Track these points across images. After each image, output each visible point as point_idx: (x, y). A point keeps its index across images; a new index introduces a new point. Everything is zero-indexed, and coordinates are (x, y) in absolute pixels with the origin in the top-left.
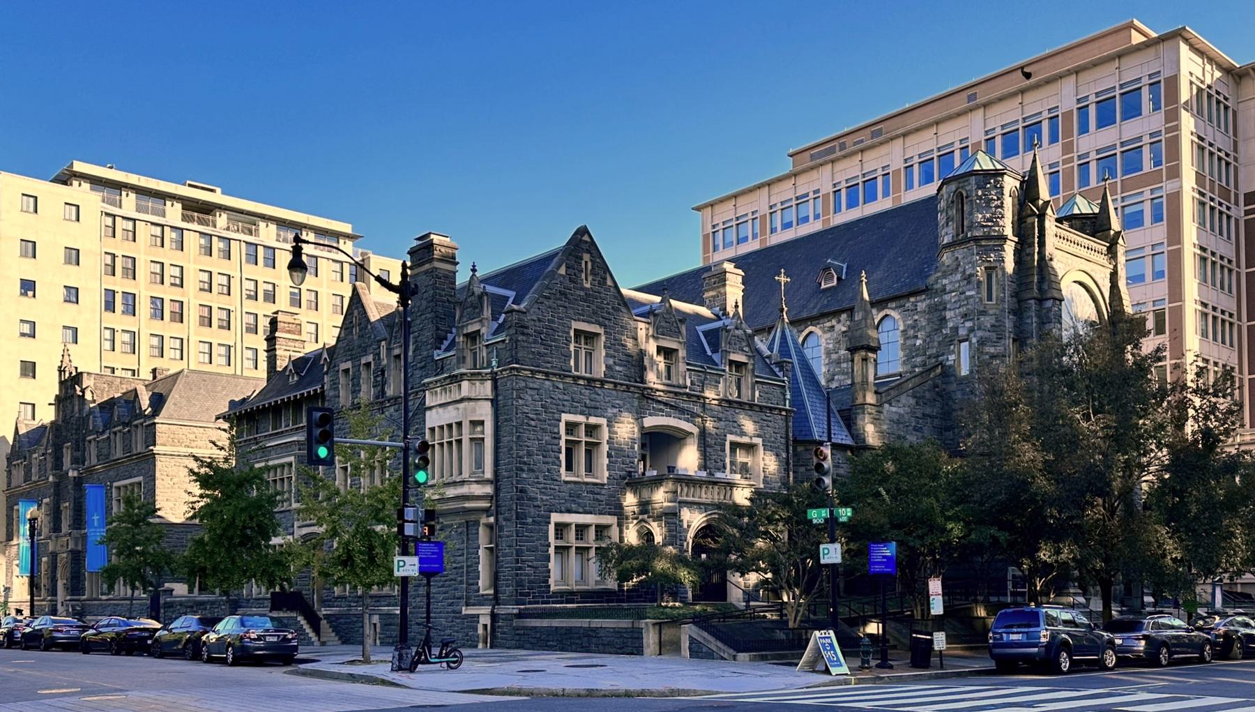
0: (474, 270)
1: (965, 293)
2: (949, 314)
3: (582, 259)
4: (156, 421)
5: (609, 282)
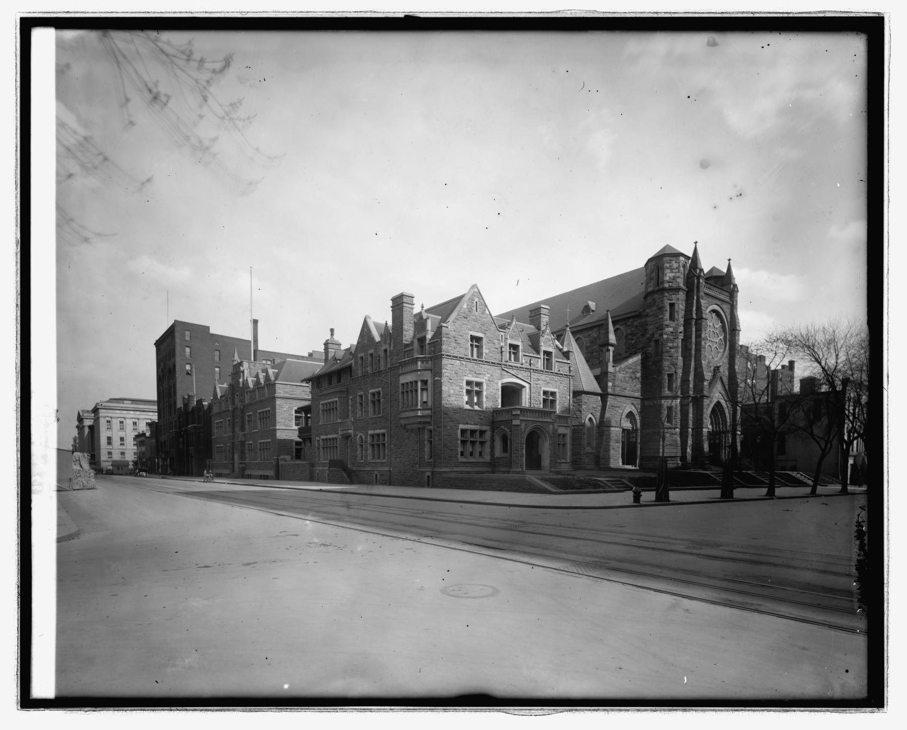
0: (422, 307)
1: (658, 316)
2: (649, 327)
3: (474, 300)
4: (276, 382)
5: (487, 312)
